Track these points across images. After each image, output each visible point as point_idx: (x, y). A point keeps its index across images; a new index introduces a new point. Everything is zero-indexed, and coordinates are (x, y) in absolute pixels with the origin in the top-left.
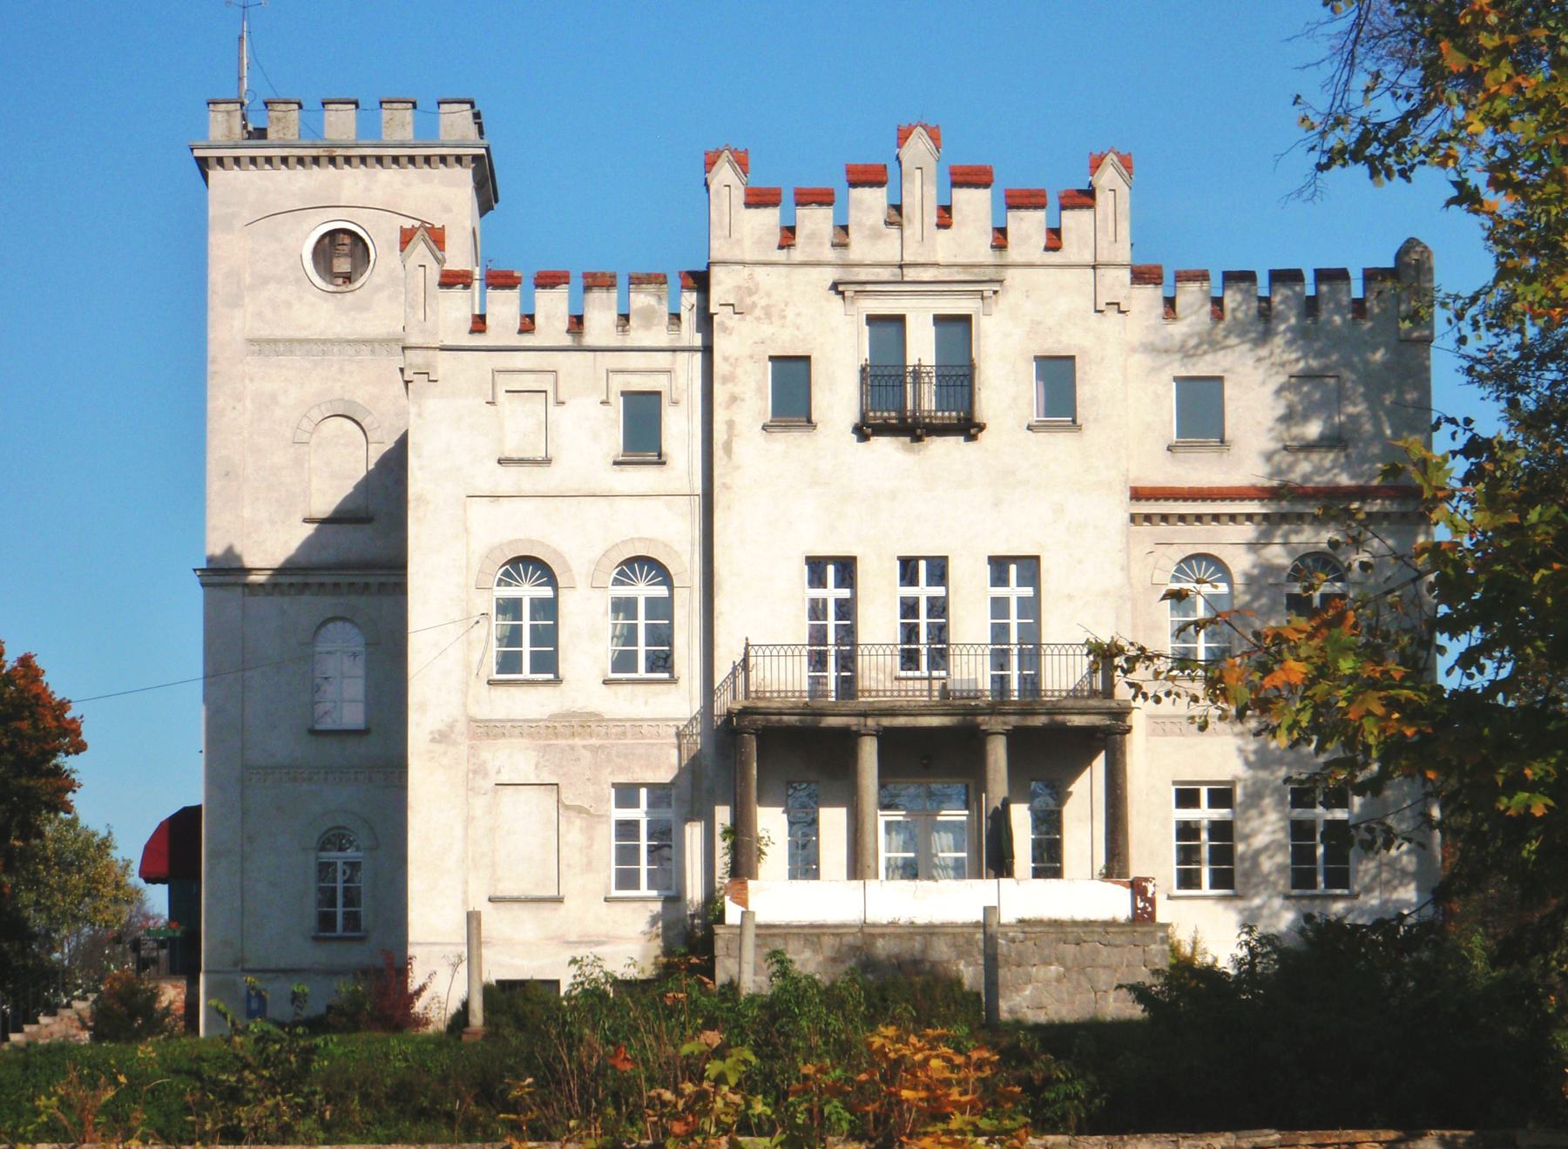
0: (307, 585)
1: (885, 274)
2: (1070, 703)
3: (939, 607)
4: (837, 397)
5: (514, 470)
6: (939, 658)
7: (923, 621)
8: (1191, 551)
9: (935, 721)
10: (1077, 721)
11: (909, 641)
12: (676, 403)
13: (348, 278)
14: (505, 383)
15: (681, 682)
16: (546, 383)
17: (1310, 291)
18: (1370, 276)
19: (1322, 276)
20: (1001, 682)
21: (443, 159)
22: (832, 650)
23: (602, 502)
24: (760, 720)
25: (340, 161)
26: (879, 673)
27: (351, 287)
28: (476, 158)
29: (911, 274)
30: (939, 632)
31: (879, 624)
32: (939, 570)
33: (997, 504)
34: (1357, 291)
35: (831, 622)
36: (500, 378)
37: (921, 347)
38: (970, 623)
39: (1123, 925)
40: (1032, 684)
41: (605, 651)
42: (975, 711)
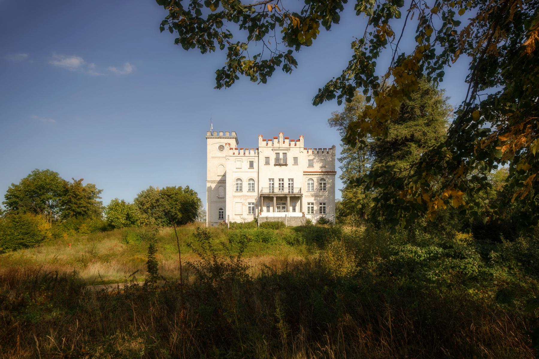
3: (283, 184)
4: (272, 162)
6: (283, 189)
20: (289, 192)
31: (276, 185)
37: (281, 156)
38: (286, 185)
40: (292, 192)
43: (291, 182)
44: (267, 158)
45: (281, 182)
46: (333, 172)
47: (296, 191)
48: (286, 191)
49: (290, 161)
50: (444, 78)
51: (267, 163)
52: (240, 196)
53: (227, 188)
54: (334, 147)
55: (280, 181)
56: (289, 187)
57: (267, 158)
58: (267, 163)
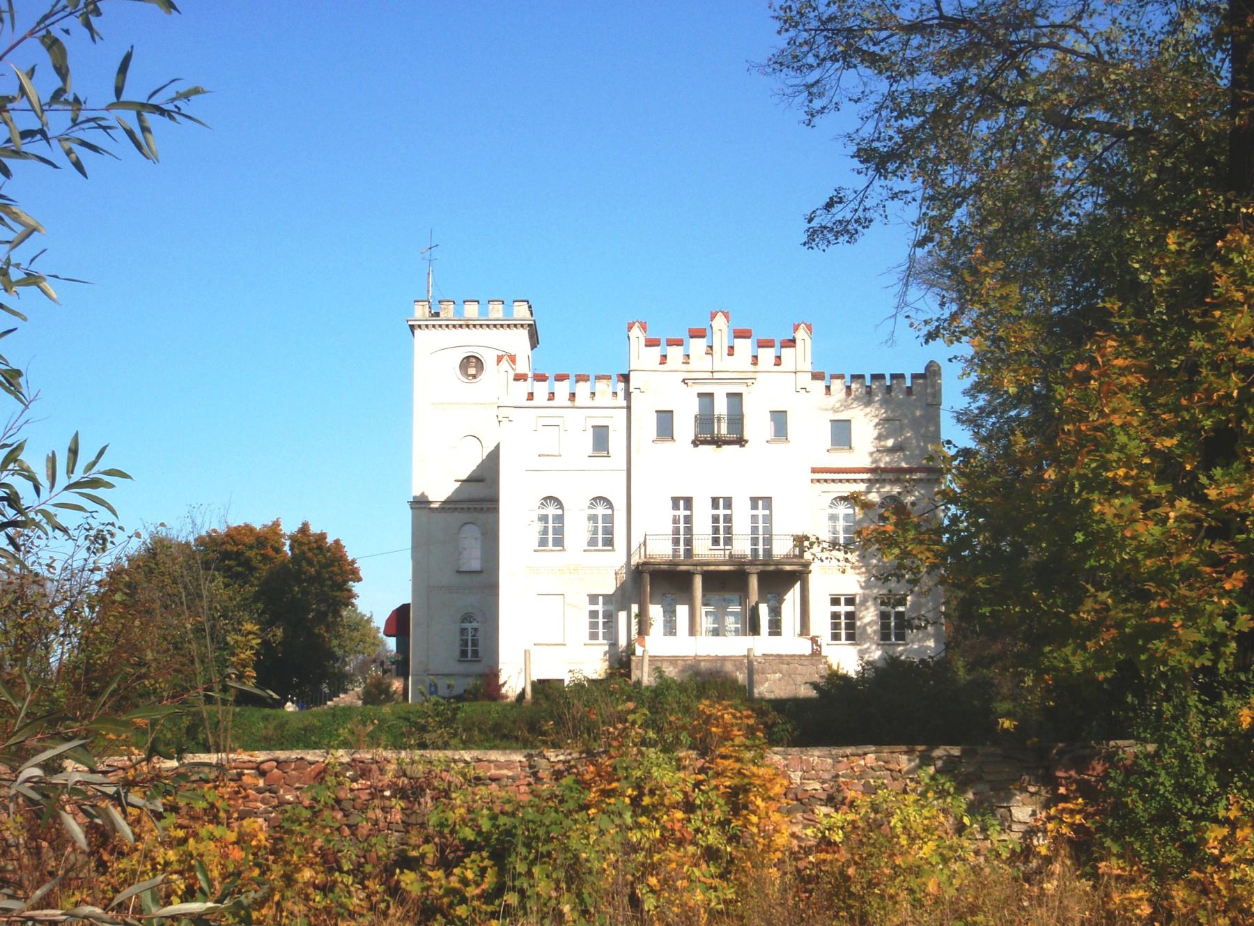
3: (728, 519)
4: (685, 427)
6: (728, 541)
10: (788, 568)
13: (474, 377)
20: (755, 551)
24: (651, 568)
29: (716, 375)
30: (728, 530)
32: (728, 503)
40: (768, 552)
42: (744, 564)
45: (722, 512)
47: (782, 548)
48: (742, 546)
49: (756, 425)
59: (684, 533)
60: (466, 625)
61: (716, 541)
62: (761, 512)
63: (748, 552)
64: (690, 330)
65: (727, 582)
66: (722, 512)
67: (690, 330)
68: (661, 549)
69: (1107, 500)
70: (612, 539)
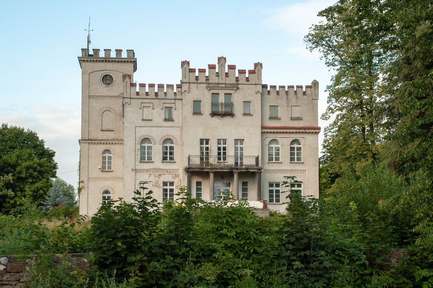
0: (101, 143)
1: (215, 85)
2: (250, 167)
3: (225, 149)
4: (206, 109)
5: (144, 122)
6: (225, 159)
7: (222, 151)
8: (294, 139)
9: (225, 170)
10: (252, 170)
11: (202, 155)
12: (175, 109)
13: (109, 84)
14: (143, 105)
15: (162, 164)
16: (151, 105)
17: (295, 90)
18: (307, 87)
19: (298, 87)
20: (236, 163)
21: (100, 61)
22: (107, 160)
23: (161, 128)
24: (192, 170)
25: (108, 61)
26: (213, 160)
27: (109, 86)
28: (134, 61)
29: (220, 85)
30: (225, 153)
31: (214, 152)
32: (225, 141)
33: (236, 129)
34: (286, 89)
35: (222, 151)
36: (164, 104)
37: (222, 99)
38: (231, 152)
39: (261, 209)
40: (242, 164)
41: (161, 156)
42: (232, 169)
43: (222, 146)
44: (197, 103)
45: (205, 146)
46: (314, 128)
47: (249, 162)
48: (230, 161)
49: (238, 109)
50: (237, 91)
51: (197, 112)
52: (147, 171)
53: (318, 189)
54: (315, 84)
55: (202, 143)
56: (219, 154)
57: (197, 103)
58: (197, 112)
59: (205, 155)
60: (105, 195)
61: (219, 159)
62: (205, 146)
63: (234, 163)
64: (209, 65)
65: (224, 175)
66: (222, 146)
67: (209, 65)
68: (196, 161)
69: (92, 276)
70: (291, 150)
